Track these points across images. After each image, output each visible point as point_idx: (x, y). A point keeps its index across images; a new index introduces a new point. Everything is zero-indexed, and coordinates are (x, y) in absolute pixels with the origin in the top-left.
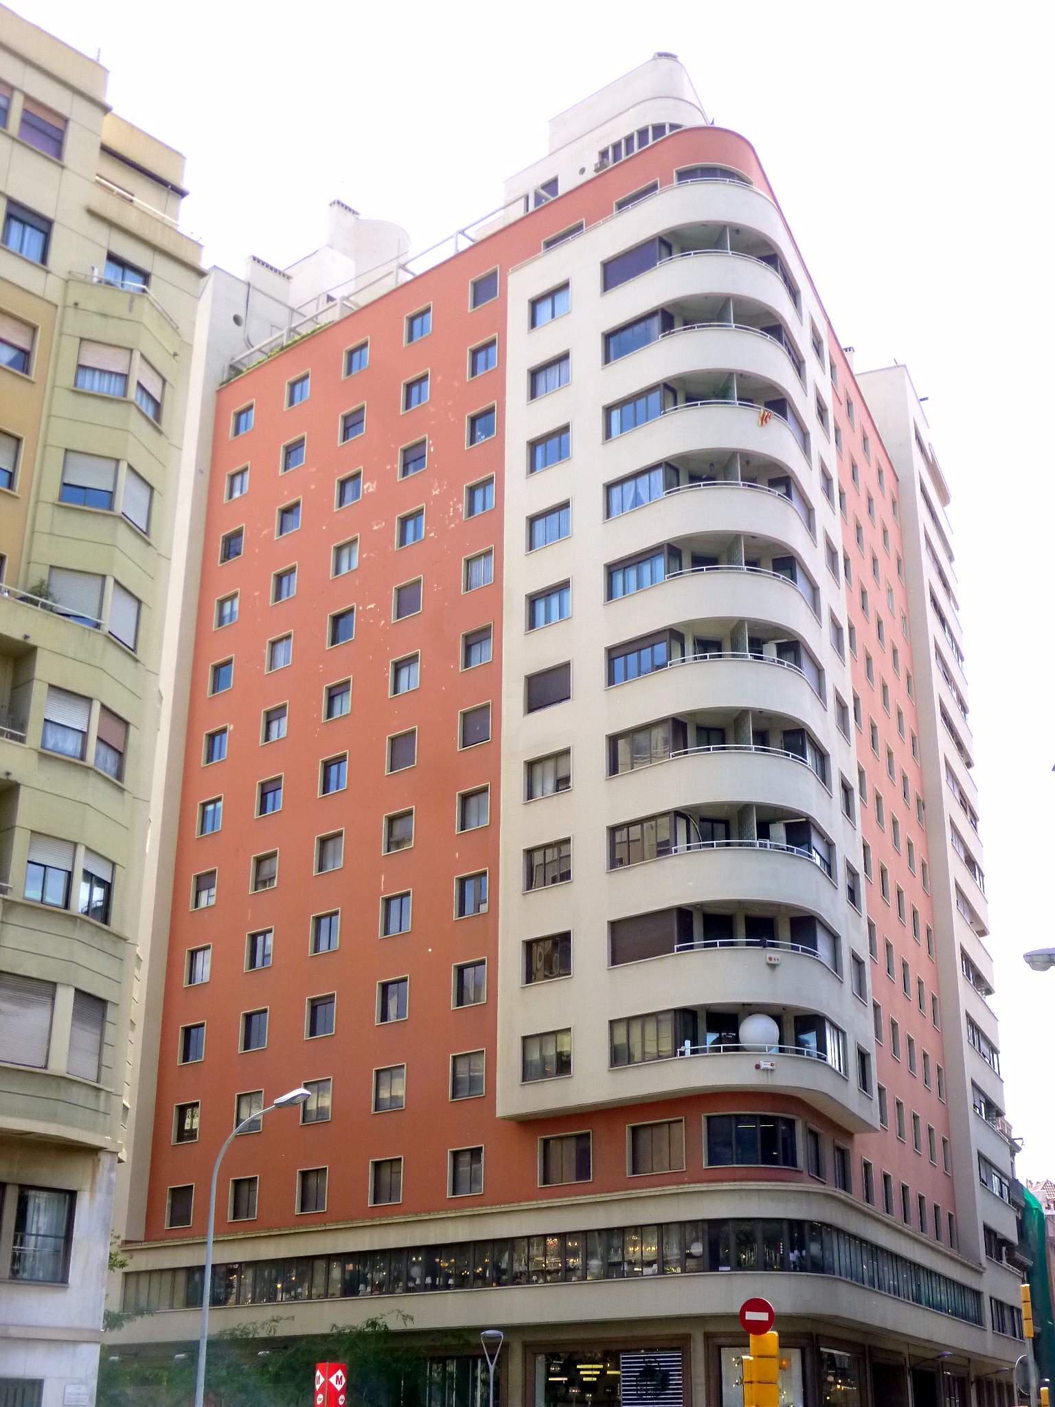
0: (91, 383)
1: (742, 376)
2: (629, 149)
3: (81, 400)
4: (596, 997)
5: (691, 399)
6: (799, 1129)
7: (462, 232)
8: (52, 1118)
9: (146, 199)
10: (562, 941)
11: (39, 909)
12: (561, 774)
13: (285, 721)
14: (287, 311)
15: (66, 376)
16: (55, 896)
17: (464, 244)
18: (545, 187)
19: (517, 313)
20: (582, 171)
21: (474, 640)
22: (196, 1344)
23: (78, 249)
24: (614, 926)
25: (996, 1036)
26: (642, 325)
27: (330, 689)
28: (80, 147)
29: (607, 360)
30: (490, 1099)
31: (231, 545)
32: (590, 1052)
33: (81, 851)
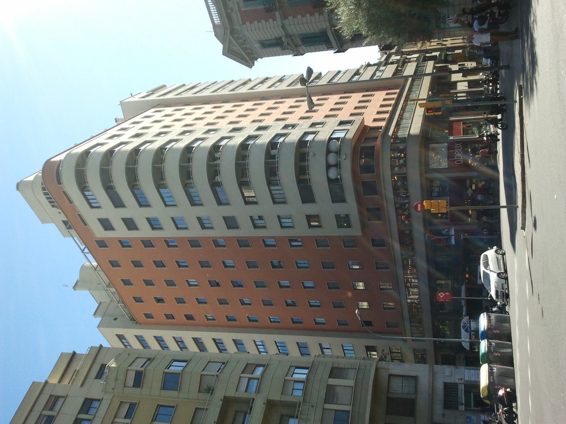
1: (127, 164)
5: (136, 180)
6: (363, 145)
7: (83, 251)
9: (77, 365)
10: (200, 219)
11: (305, 390)
13: (244, 299)
14: (112, 303)
16: (301, 386)
17: (86, 250)
18: (66, 225)
19: (109, 234)
20: (59, 213)
21: (216, 244)
23: (95, 389)
25: (333, 72)
31: (189, 317)
32: (341, 209)
33: (287, 378)
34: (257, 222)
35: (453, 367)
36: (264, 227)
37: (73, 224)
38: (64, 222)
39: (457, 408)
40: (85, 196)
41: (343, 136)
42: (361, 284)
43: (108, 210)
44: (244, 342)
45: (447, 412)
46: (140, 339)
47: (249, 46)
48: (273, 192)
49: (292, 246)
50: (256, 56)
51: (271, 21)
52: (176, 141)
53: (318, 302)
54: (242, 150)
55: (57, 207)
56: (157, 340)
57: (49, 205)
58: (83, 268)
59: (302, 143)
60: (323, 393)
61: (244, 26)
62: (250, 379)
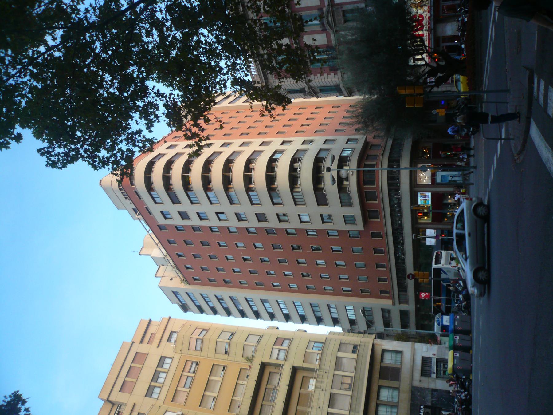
0: (199, 348)
3: (203, 350)
4: (335, 208)
8: (366, 357)
15: (198, 353)
17: (160, 245)
22: (492, 122)
23: (168, 349)
24: (318, 205)
28: (143, 348)
30: (360, 231)
32: (348, 211)
34: (280, 218)
35: (429, 345)
37: (141, 211)
38: (134, 209)
39: (430, 376)
45: (424, 378)
46: (315, 309)
48: (295, 197)
49: (308, 235)
56: (312, 306)
60: (334, 363)
62: (280, 350)
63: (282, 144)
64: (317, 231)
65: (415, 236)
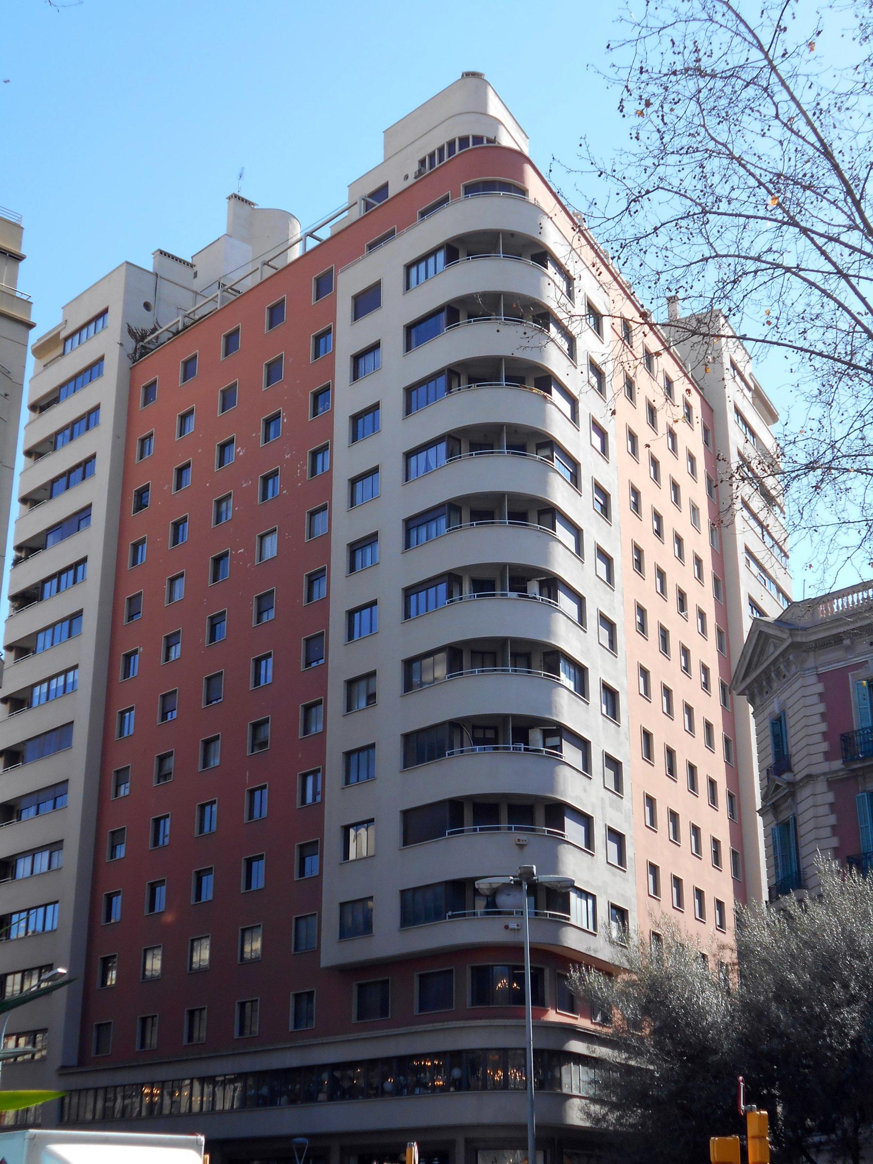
2: (451, 151)
7: (310, 234)
10: (372, 539)
12: (371, 692)
13: (179, 646)
17: (268, 272)
18: (372, 195)
19: (344, 307)
20: (406, 177)
21: (312, 579)
26: (433, 320)
27: (309, 576)
29: (408, 348)
30: (316, 953)
31: (141, 499)
34: (359, 759)
36: (349, 708)
37: (379, 212)
38: (385, 187)
40: (433, 252)
41: (573, 921)
42: (257, 945)
43: (400, 308)
44: (73, 642)
47: (775, 685)
49: (304, 777)
50: (758, 701)
51: (824, 747)
52: (575, 480)
53: (167, 840)
54: (546, 654)
55: (420, 172)
56: (90, 413)
57: (425, 153)
58: (285, 217)
59: (558, 812)
61: (814, 679)
63: (598, 489)
64: (319, 807)
65: (300, 1148)
